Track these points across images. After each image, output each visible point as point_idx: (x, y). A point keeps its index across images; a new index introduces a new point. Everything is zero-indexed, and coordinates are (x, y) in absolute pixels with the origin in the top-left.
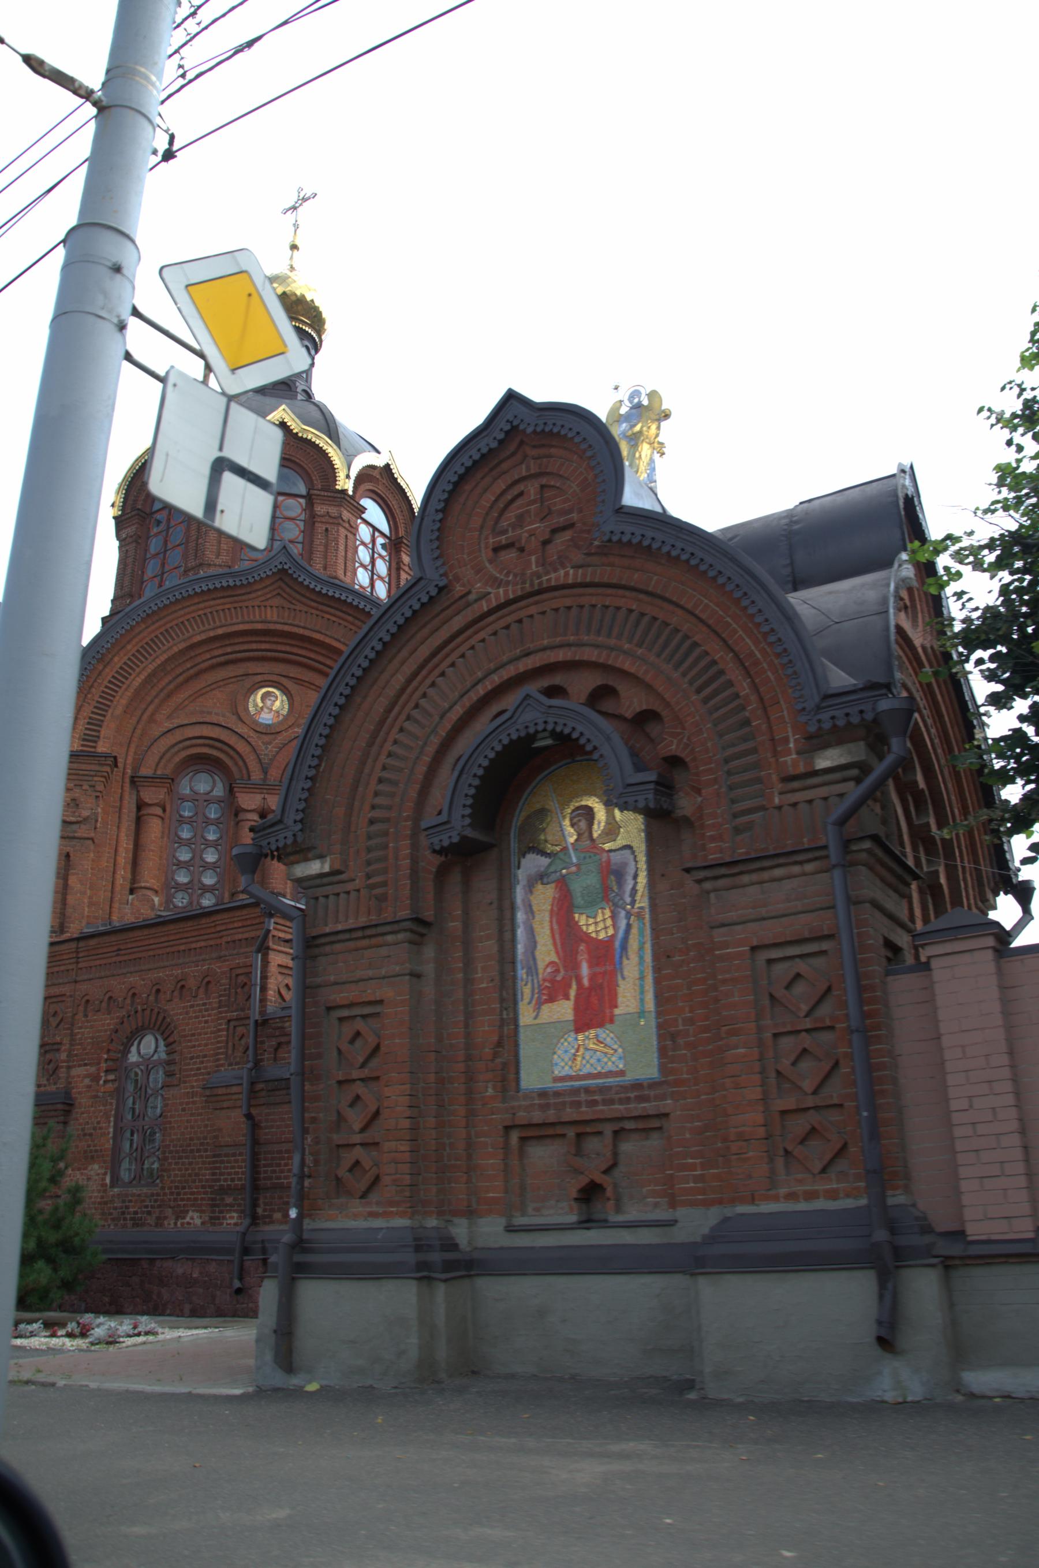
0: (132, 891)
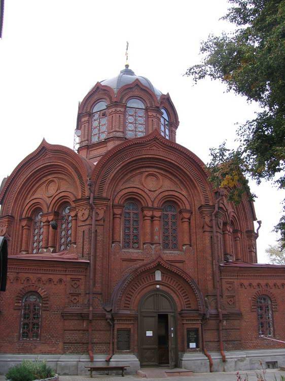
0: (113, 242)
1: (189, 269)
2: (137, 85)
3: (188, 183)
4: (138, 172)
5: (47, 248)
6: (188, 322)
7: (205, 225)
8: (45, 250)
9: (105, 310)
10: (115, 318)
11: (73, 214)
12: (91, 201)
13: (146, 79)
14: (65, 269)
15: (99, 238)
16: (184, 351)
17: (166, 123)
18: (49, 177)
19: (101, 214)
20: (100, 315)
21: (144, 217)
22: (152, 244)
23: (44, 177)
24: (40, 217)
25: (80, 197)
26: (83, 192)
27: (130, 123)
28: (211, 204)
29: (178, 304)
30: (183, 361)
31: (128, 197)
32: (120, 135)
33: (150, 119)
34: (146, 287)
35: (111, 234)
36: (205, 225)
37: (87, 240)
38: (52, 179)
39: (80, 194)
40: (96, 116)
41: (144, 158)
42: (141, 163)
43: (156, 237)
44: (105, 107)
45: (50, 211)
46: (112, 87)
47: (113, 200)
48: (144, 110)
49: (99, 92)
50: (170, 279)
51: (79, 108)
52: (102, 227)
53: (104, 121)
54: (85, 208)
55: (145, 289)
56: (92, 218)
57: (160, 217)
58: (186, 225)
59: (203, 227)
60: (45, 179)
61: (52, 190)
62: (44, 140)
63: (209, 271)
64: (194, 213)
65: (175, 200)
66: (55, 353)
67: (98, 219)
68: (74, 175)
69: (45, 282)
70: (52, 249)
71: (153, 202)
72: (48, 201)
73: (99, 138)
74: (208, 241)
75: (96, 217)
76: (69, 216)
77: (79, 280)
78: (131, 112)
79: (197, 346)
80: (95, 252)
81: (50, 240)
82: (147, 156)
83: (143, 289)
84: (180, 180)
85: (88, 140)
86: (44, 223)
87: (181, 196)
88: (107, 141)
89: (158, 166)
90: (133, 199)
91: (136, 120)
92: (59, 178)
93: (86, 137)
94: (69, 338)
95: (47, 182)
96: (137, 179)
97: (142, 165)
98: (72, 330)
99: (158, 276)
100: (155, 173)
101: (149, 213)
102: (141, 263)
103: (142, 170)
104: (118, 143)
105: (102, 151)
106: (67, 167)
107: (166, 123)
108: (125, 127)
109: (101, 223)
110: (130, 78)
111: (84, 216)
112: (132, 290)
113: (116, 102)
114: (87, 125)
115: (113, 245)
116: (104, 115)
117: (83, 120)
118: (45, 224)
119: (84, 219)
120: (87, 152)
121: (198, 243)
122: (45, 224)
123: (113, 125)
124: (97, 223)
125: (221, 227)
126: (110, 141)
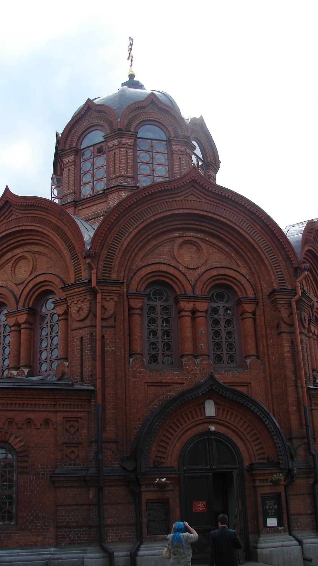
0: (131, 356)
1: (258, 393)
2: (153, 102)
3: (249, 254)
4: (167, 237)
5: (17, 368)
6: (262, 484)
7: (282, 322)
8: (15, 373)
9: (125, 469)
10: (142, 483)
11: (61, 310)
12: (94, 284)
13: (165, 95)
14: (54, 403)
15: (109, 348)
16: (258, 533)
17: (200, 163)
18: (17, 251)
19: (111, 306)
20: (117, 477)
21: (179, 313)
22: (196, 357)
23: (7, 252)
24: (4, 318)
25: (72, 282)
26: (78, 272)
27: (143, 163)
28: (289, 287)
29: (245, 455)
30: (259, 550)
31: (149, 281)
32: (125, 182)
33: (176, 157)
34: (191, 428)
35: (127, 341)
36: (282, 322)
37: (87, 352)
38: (20, 255)
39: (72, 277)
40: (88, 154)
41: (176, 214)
42: (172, 224)
43: (202, 346)
44: (102, 139)
45: (20, 307)
46: (112, 106)
47: (128, 286)
48: (165, 143)
49: (89, 114)
50: (229, 414)
51: (58, 142)
52: (113, 329)
53: (100, 161)
54: (82, 299)
55: (189, 432)
56: (95, 316)
57: (206, 312)
58: (249, 324)
59: (278, 326)
60: (10, 255)
61: (23, 272)
62: (7, 189)
63: (291, 398)
64: (261, 304)
65: (228, 283)
66: (44, 545)
67: (105, 316)
68: (60, 245)
69: (39, 426)
70: (26, 371)
71: (193, 287)
72: (17, 291)
73: (93, 188)
74: (286, 348)
75: (102, 314)
76: (53, 315)
77: (77, 420)
78: (144, 145)
79: (280, 523)
80: (103, 373)
81: (22, 354)
82: (181, 211)
83: (187, 431)
84: (235, 249)
85: (75, 193)
86: (10, 327)
87: (238, 277)
88: (105, 193)
89: (199, 227)
90: (161, 285)
91: (153, 158)
92: (34, 252)
93: (72, 188)
94: (66, 519)
95: (14, 259)
96: (165, 248)
97: (174, 227)
98: (69, 505)
99: (210, 410)
100: (195, 239)
101: (188, 306)
102: (179, 389)
103: (173, 235)
104: (125, 194)
105: (100, 208)
106: (47, 233)
107: (200, 163)
108: (135, 169)
109: (111, 322)
110: (136, 93)
111: (81, 312)
112: (167, 434)
113: (119, 129)
114: (72, 168)
115: (131, 360)
116: (100, 151)
117: (66, 160)
118: (13, 328)
119: (82, 317)
120: (75, 211)
121: (270, 353)
122: (13, 328)
123: (117, 167)
124: (104, 323)
125: (306, 326)
126: (111, 193)
